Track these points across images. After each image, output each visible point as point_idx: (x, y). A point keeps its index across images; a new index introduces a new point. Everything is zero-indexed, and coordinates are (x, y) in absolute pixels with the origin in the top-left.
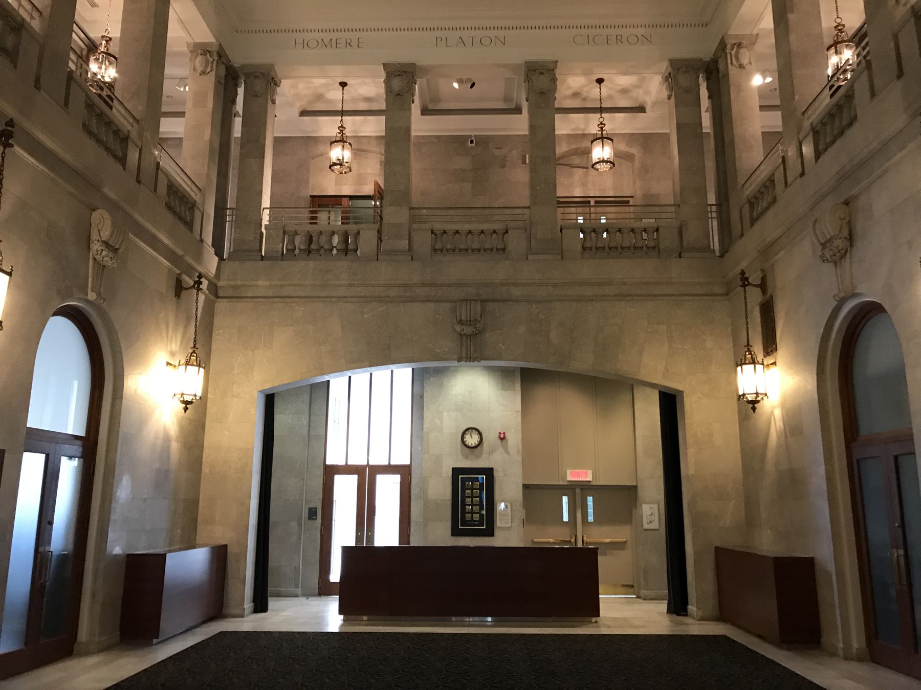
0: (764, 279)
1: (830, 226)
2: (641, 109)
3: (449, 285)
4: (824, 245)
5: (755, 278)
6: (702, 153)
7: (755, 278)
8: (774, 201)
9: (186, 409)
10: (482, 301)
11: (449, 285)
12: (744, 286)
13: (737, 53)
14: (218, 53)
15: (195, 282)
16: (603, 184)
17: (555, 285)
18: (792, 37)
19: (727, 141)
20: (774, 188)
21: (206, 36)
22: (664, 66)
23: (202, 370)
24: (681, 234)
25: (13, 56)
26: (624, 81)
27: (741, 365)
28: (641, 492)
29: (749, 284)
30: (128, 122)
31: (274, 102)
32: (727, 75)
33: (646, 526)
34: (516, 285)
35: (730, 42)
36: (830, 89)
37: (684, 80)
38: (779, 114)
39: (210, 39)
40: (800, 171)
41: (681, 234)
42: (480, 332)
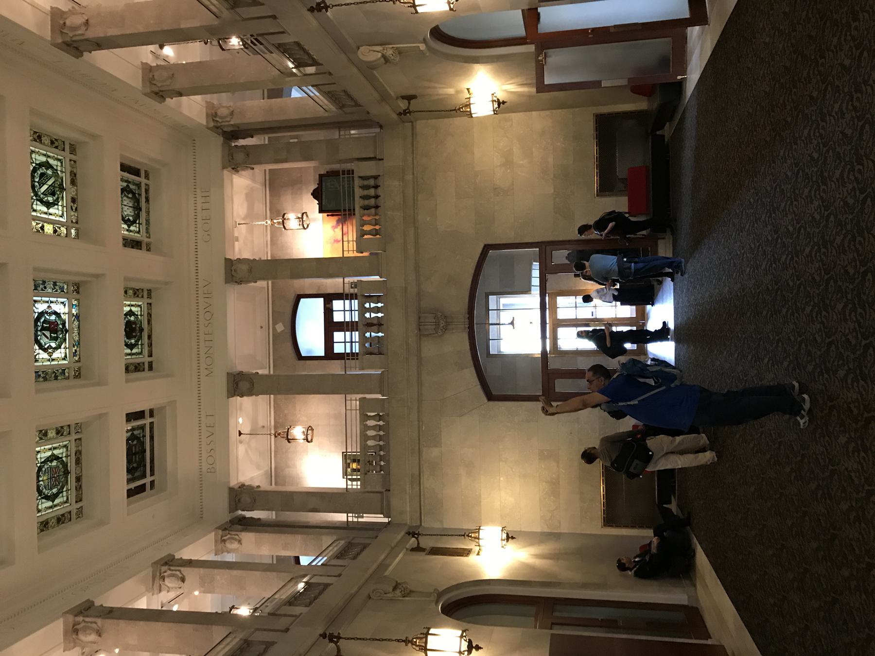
0: (403, 97)
5: (403, 105)
8: (298, 44)
9: (478, 648)
12: (410, 112)
13: (221, 118)
14: (76, 616)
15: (331, 641)
20: (284, 44)
21: (211, 537)
23: (432, 631)
25: (269, 645)
27: (471, 114)
29: (408, 108)
30: (231, 641)
31: (258, 487)
36: (255, 45)
37: (239, 157)
39: (213, 533)
40: (271, 19)
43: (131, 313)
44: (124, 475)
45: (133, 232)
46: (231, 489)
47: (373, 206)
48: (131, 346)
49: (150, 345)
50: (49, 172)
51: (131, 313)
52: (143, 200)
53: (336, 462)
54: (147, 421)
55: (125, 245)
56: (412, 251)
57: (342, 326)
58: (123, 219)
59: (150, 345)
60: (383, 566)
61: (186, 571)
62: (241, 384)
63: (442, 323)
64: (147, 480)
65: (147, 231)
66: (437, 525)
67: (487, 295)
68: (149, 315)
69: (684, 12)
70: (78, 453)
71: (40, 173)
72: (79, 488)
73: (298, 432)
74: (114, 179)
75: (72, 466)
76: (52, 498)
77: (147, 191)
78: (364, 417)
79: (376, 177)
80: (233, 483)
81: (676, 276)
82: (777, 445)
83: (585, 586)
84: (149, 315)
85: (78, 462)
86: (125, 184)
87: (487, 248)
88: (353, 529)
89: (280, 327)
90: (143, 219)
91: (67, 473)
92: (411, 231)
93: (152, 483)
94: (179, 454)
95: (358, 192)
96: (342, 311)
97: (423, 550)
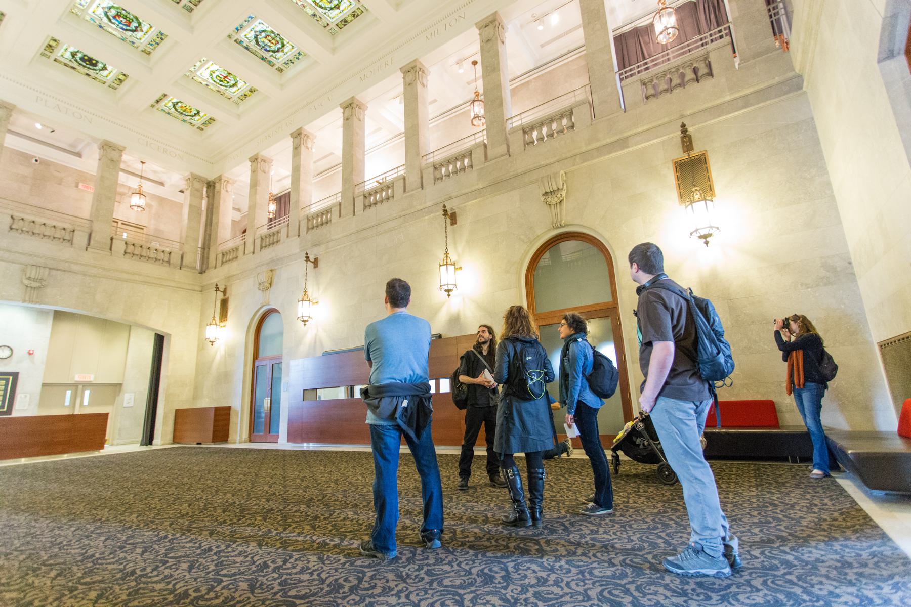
0: (225, 289)
1: (264, 278)
2: (162, 184)
3: (21, 254)
4: (260, 284)
5: (221, 288)
6: (200, 222)
7: (221, 288)
10: (50, 269)
11: (21, 254)
16: (132, 217)
17: (104, 269)
18: (258, 197)
19: (214, 221)
22: (187, 174)
24: (182, 258)
26: (156, 167)
28: (124, 387)
32: (219, 192)
33: (125, 405)
34: (76, 264)
35: (224, 178)
37: (197, 185)
38: (441, 381)
41: (182, 258)
42: (44, 287)
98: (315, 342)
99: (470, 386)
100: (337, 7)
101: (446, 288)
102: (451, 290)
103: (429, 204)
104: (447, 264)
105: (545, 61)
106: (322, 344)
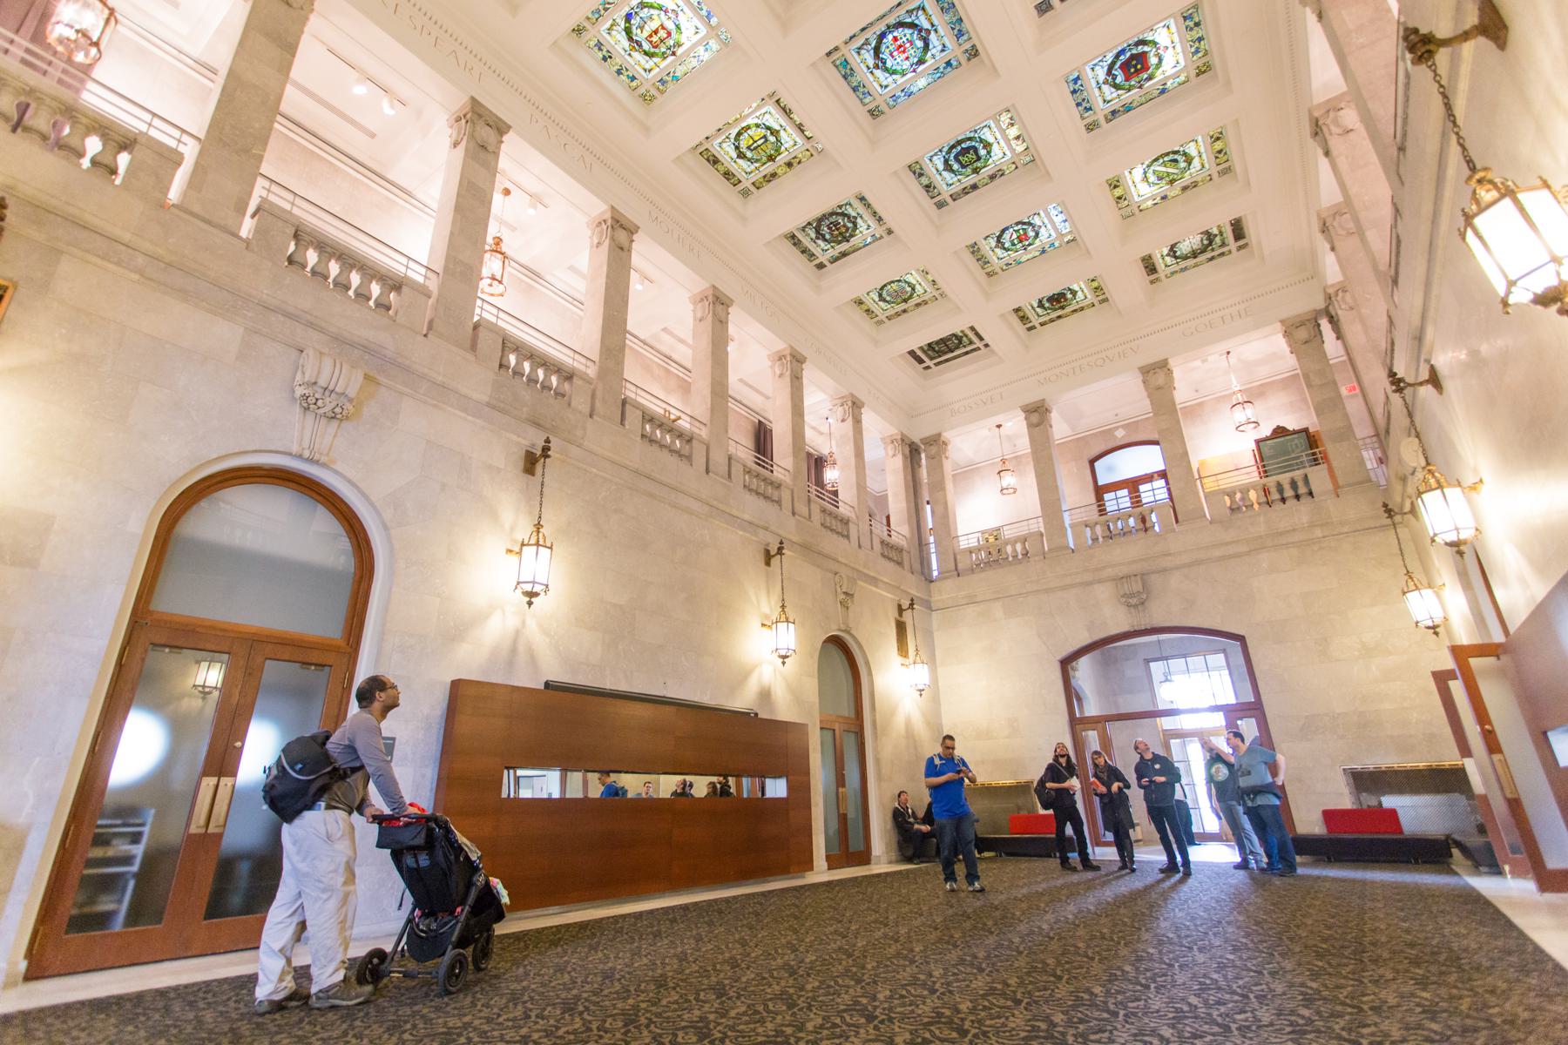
21: (893, 431)
37: (1302, 334)
43: (1074, 293)
44: (924, 342)
45: (1163, 262)
46: (939, 435)
47: (1273, 497)
48: (1041, 305)
49: (1052, 321)
50: (1183, 165)
51: (1074, 293)
52: (1209, 255)
53: (991, 523)
54: (978, 344)
55: (1143, 260)
56: (1217, 553)
57: (1136, 501)
58: (1173, 246)
59: (1052, 321)
60: (874, 581)
61: (850, 421)
62: (1037, 414)
63: (1134, 601)
64: (928, 362)
65: (1173, 273)
66: (935, 626)
67: (1224, 651)
68: (1082, 309)
69: (1553, 862)
70: (925, 302)
71: (1175, 157)
72: (898, 314)
73: (1009, 480)
74: (1218, 219)
75: (912, 302)
76: (882, 299)
77: (1222, 254)
78: (1024, 540)
79: (1311, 494)
80: (946, 435)
81: (1242, 872)
82: (1112, 1007)
83: (877, 761)
84: (1082, 309)
85: (918, 305)
86: (1215, 231)
87: (1241, 639)
88: (921, 551)
89: (1120, 433)
90: (1183, 264)
91: (905, 301)
92: (1243, 548)
93: (928, 368)
94: (958, 378)
95: (1285, 478)
96: (1153, 493)
97: (900, 614)
98: (514, 650)
99: (1057, 790)
100: (741, 155)
101: (528, 588)
102: (537, 594)
103: (746, 517)
104: (537, 544)
105: (327, 137)
106: (533, 660)
